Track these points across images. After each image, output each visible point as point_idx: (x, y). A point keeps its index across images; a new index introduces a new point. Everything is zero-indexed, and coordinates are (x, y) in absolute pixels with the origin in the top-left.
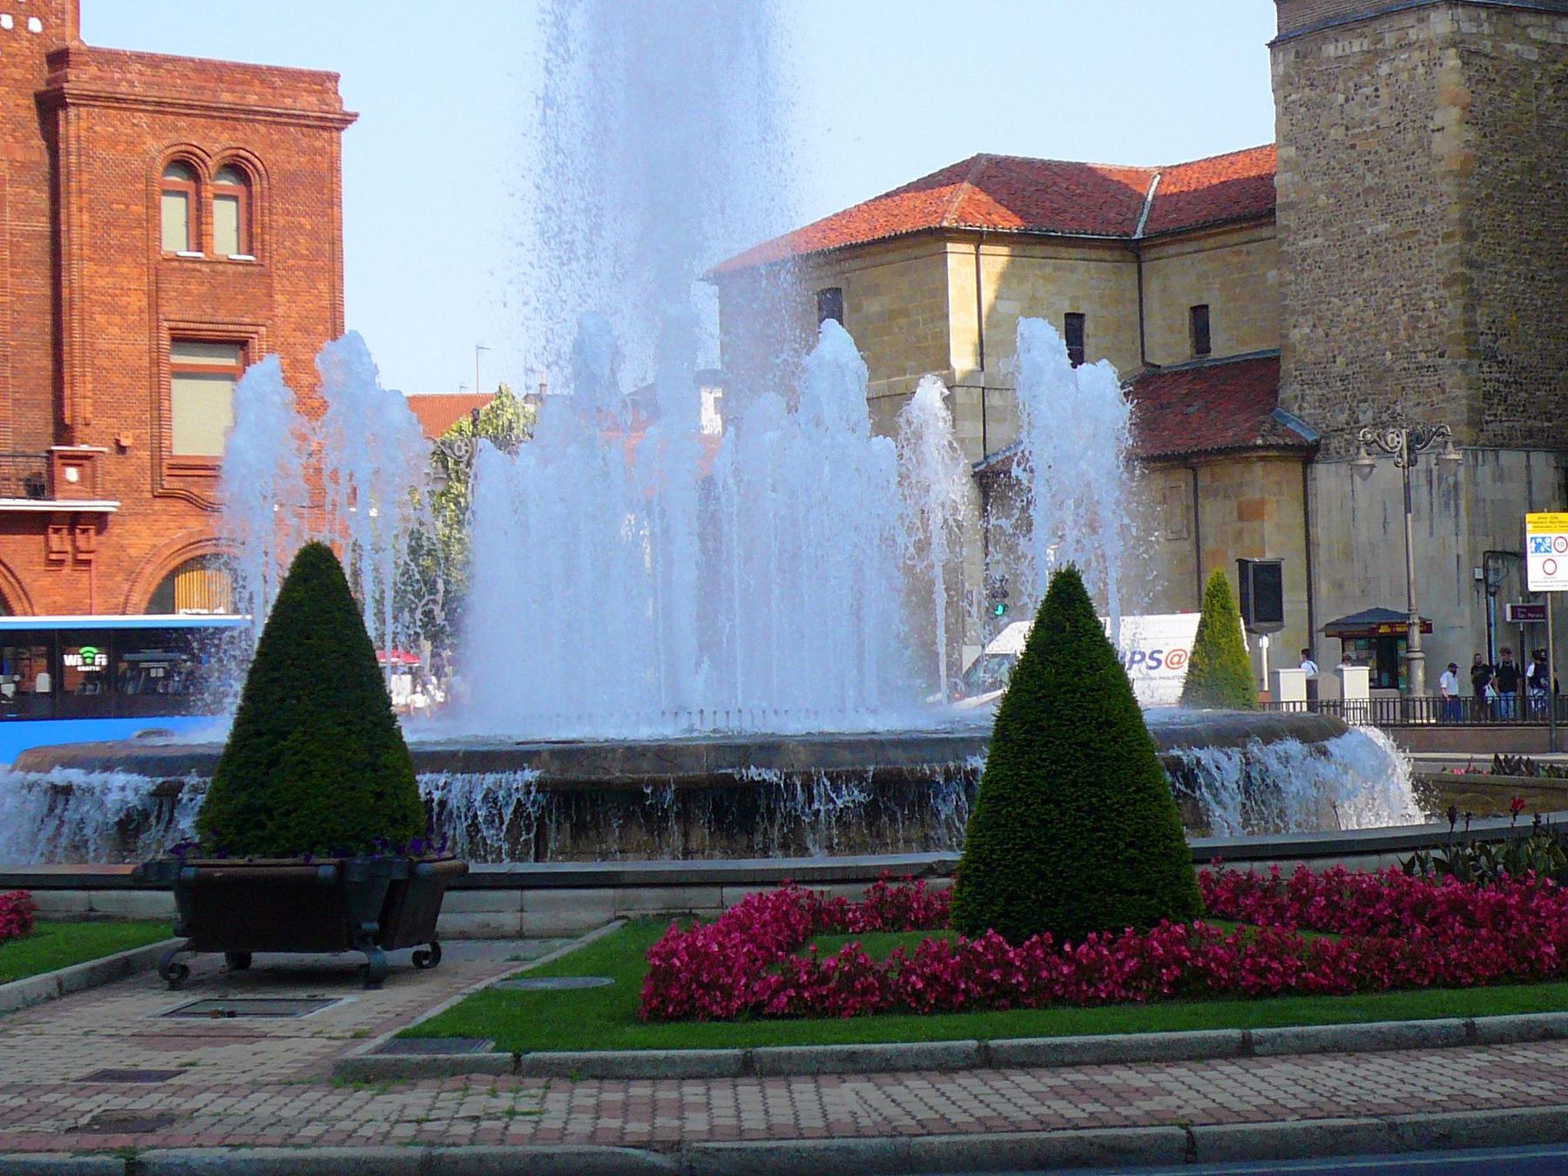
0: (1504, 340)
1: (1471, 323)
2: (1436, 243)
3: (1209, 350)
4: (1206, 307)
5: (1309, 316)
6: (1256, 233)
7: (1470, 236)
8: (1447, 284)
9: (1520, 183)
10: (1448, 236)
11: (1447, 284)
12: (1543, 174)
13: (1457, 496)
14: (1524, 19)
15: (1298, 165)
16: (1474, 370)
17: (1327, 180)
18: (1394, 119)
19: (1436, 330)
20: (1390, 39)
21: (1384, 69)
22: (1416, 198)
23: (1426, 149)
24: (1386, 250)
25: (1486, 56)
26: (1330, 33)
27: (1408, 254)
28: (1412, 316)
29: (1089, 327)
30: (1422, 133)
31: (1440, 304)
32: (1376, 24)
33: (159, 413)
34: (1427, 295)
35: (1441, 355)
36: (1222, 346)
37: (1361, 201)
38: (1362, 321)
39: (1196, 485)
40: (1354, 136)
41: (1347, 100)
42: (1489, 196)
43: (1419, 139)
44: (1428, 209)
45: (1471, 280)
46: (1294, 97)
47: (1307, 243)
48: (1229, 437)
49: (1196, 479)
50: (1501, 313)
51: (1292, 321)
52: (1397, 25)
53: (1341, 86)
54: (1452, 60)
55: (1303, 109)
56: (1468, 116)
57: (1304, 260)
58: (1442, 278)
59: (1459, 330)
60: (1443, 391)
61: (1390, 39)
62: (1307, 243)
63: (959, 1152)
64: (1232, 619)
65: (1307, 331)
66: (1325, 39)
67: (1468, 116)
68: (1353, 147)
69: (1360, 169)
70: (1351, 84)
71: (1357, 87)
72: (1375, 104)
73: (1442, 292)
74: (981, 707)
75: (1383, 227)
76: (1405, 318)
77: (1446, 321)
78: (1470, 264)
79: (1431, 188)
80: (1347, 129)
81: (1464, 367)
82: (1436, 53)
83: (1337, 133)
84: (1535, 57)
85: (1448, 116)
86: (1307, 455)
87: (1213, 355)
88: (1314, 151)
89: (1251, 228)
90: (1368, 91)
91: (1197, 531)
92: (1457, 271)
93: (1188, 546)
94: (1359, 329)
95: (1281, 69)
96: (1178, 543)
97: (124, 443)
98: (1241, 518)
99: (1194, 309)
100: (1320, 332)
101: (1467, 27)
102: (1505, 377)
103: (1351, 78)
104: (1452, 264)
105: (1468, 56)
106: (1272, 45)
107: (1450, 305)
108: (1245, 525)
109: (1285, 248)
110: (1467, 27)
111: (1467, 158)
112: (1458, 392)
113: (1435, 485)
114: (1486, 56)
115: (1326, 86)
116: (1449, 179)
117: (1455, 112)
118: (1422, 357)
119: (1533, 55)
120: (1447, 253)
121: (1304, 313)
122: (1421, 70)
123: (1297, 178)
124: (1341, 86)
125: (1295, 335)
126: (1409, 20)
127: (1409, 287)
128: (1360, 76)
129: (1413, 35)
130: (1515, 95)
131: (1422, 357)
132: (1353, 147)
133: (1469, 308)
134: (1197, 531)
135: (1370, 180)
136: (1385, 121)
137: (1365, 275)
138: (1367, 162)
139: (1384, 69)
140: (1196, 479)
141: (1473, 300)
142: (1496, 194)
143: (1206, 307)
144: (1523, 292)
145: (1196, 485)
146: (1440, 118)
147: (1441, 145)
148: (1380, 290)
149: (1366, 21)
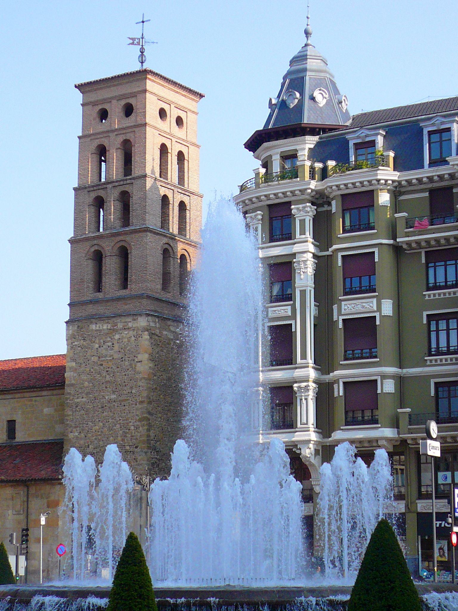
0: (158, 443)
1: (149, 436)
2: (136, 404)
3: (15, 438)
4: (15, 421)
5: (78, 429)
6: (40, 393)
7: (150, 403)
8: (140, 420)
9: (165, 384)
10: (142, 402)
11: (140, 420)
12: (172, 381)
13: (141, 503)
14: (169, 323)
15: (76, 369)
16: (149, 454)
17: (89, 376)
18: (120, 356)
19: (134, 438)
20: (120, 326)
21: (117, 337)
22: (128, 387)
23: (134, 369)
24: (114, 405)
25: (157, 335)
26: (94, 320)
27: (124, 408)
28: (124, 432)
30: (132, 362)
31: (137, 428)
32: (114, 319)
34: (131, 424)
35: (136, 447)
36: (21, 437)
37: (104, 386)
38: (102, 432)
39: (28, 494)
40: (102, 361)
41: (100, 347)
42: (156, 388)
43: (131, 365)
44: (134, 391)
45: (149, 420)
46: (76, 343)
47: (78, 400)
48: (43, 474)
49: (28, 491)
50: (158, 433)
51: (70, 430)
52: (123, 321)
53: (97, 341)
54: (146, 336)
55: (79, 348)
56: (151, 358)
57: (77, 407)
58: (138, 418)
59: (145, 438)
60: (137, 461)
61: (120, 326)
62: (78, 400)
65: (77, 434)
66: (91, 323)
67: (151, 358)
68: (102, 365)
69: (104, 374)
70: (102, 341)
71: (104, 342)
72: (112, 349)
73: (138, 423)
74: (350, 580)
75: (113, 397)
76: (121, 432)
77: (139, 434)
78: (149, 413)
79: (135, 383)
80: (99, 358)
81: (146, 453)
82: (140, 333)
83: (95, 359)
85: (144, 357)
87: (17, 440)
88: (84, 365)
89: (40, 391)
90: (110, 344)
91: (27, 511)
92: (145, 415)
93: (22, 517)
94: (99, 435)
96: (18, 516)
99: (9, 421)
100: (83, 435)
101: (152, 324)
102: (158, 457)
103: (101, 339)
104: (142, 413)
105: (152, 335)
106: (66, 322)
107: (141, 428)
109: (69, 401)
110: (152, 324)
112: (143, 462)
113: (132, 498)
114: (157, 335)
115: (91, 340)
116: (143, 381)
117: (146, 356)
118: (128, 448)
120: (141, 408)
121: (76, 427)
122: (133, 338)
123: (75, 375)
124: (97, 341)
125: (71, 436)
126: (129, 319)
127: (123, 420)
128: (106, 338)
129: (130, 325)
130: (165, 351)
131: (128, 448)
132: (102, 365)
133: (148, 430)
134: (27, 511)
135: (108, 378)
136: (116, 356)
137: (104, 415)
138: (107, 371)
139: (117, 337)
140: (28, 491)
142: (158, 388)
143: (15, 421)
144: (165, 425)
145: (28, 494)
146: (140, 357)
147: (140, 367)
148: (110, 421)
149: (108, 318)
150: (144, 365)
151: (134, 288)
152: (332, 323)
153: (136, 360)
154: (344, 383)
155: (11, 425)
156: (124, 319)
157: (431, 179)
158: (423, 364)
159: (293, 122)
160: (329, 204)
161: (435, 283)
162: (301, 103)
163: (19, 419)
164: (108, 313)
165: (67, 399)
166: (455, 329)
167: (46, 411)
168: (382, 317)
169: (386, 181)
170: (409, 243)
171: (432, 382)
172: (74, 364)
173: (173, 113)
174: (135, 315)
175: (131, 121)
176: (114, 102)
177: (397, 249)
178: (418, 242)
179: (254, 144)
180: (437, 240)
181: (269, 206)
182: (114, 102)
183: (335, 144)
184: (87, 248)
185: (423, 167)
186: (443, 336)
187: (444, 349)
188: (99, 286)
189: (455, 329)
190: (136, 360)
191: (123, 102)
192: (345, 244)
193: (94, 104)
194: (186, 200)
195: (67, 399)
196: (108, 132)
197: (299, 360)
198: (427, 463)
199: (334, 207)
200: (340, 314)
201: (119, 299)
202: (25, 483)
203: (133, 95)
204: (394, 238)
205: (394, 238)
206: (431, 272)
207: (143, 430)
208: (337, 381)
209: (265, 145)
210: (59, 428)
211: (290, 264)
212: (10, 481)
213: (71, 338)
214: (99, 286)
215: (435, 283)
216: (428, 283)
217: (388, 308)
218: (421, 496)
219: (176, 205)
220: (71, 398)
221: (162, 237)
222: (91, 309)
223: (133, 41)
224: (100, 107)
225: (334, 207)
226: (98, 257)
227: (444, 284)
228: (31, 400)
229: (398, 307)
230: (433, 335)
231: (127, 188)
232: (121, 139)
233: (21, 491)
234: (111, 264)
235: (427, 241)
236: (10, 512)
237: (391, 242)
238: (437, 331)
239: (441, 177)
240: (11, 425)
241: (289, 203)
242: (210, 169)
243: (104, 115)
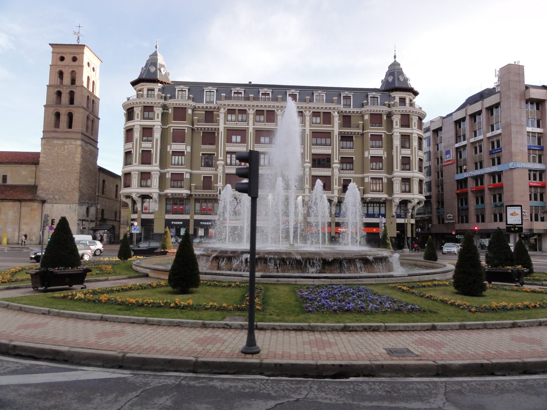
21: (66, 147)
29: (105, 212)
31: (75, 182)
36: (9, 182)
48: (29, 197)
54: (80, 148)
59: (78, 187)
61: (68, 143)
63: (133, 309)
64: (459, 321)
75: (64, 170)
83: (56, 154)
86: (43, 202)
93: (18, 214)
97: (24, 238)
105: (82, 148)
126: (73, 141)
135: (61, 162)
136: (66, 154)
139: (66, 147)
141: (80, 182)
146: (77, 156)
147: (77, 160)
150: (78, 159)
151: (74, 128)
152: (167, 152)
154: (171, 174)
157: (207, 107)
158: (200, 170)
159: (153, 77)
160: (168, 110)
162: (156, 71)
164: (62, 137)
167: (23, 173)
168: (187, 152)
170: (198, 128)
171: (202, 176)
172: (44, 155)
173: (92, 66)
174: (76, 139)
175: (76, 63)
176: (68, 55)
177: (193, 130)
178: (201, 128)
179: (134, 84)
180: (208, 129)
181: (144, 106)
182: (68, 55)
183: (169, 89)
184: (52, 110)
185: (203, 103)
188: (57, 125)
191: (72, 56)
192: (174, 125)
193: (58, 53)
196: (65, 66)
197: (154, 163)
199: (170, 111)
200: (171, 148)
201: (68, 132)
202: (20, 201)
203: (78, 54)
204: (193, 125)
205: (193, 125)
207: (77, 184)
208: (168, 172)
209: (142, 84)
211: (152, 128)
212: (10, 200)
213: (43, 145)
214: (57, 125)
217: (189, 149)
218: (195, 214)
223: (75, 33)
224: (61, 55)
225: (170, 111)
229: (192, 149)
231: (73, 90)
232: (71, 70)
233: (17, 204)
235: (205, 128)
236: (11, 212)
239: (211, 107)
240: (5, 178)
241: (133, 108)
242: (111, 89)
243: (62, 59)
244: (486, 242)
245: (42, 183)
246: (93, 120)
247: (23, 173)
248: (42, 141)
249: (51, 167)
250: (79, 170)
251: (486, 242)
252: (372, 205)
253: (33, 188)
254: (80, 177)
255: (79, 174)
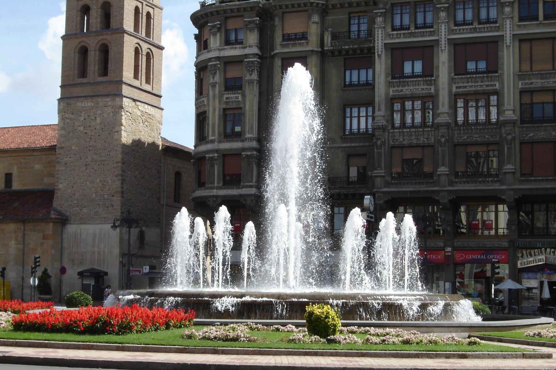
1: (122, 188)
7: (123, 163)
33: (367, 194)
34: (109, 178)
36: (16, 186)
42: (128, 152)
43: (109, 134)
47: (67, 159)
59: (120, 189)
61: (101, 104)
62: (67, 159)
84: (140, 115)
87: (13, 188)
95: (61, 107)
98: (44, 239)
108: (45, 241)
111: (61, 135)
118: (106, 196)
119: (139, 113)
122: (111, 114)
124: (83, 115)
129: (109, 103)
136: (98, 127)
139: (99, 112)
141: (123, 181)
153: (114, 130)
155: (8, 178)
156: (260, 82)
161: (351, 81)
163: (15, 172)
165: (58, 158)
166: (495, 106)
167: (37, 167)
169: (318, 4)
184: (75, 43)
186: (355, 121)
187: (355, 131)
188: (83, 73)
189: (495, 106)
190: (114, 130)
194: (151, 11)
195: (58, 158)
198: (339, 213)
206: (348, 73)
207: (118, 183)
210: (46, 180)
213: (61, 111)
214: (83, 73)
215: (351, 81)
216: (345, 82)
219: (145, 14)
220: (62, 157)
221: (135, 39)
222: (77, 91)
226: (84, 52)
227: (357, 83)
228: (25, 159)
230: (348, 120)
234: (93, 58)
237: (320, 50)
238: (351, 117)
240: (8, 178)
244: (433, 91)
245: (61, 186)
246: (148, 55)
247: (37, 167)
248: (59, 104)
249: (75, 154)
250: (120, 156)
251: (433, 91)
252: (543, 206)
253: (46, 196)
254: (123, 171)
255: (120, 165)
